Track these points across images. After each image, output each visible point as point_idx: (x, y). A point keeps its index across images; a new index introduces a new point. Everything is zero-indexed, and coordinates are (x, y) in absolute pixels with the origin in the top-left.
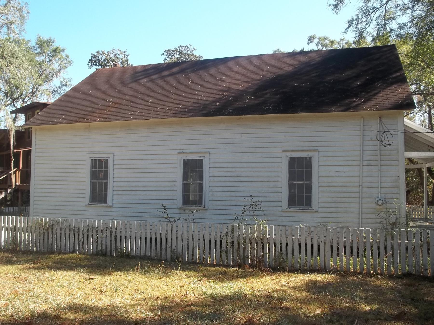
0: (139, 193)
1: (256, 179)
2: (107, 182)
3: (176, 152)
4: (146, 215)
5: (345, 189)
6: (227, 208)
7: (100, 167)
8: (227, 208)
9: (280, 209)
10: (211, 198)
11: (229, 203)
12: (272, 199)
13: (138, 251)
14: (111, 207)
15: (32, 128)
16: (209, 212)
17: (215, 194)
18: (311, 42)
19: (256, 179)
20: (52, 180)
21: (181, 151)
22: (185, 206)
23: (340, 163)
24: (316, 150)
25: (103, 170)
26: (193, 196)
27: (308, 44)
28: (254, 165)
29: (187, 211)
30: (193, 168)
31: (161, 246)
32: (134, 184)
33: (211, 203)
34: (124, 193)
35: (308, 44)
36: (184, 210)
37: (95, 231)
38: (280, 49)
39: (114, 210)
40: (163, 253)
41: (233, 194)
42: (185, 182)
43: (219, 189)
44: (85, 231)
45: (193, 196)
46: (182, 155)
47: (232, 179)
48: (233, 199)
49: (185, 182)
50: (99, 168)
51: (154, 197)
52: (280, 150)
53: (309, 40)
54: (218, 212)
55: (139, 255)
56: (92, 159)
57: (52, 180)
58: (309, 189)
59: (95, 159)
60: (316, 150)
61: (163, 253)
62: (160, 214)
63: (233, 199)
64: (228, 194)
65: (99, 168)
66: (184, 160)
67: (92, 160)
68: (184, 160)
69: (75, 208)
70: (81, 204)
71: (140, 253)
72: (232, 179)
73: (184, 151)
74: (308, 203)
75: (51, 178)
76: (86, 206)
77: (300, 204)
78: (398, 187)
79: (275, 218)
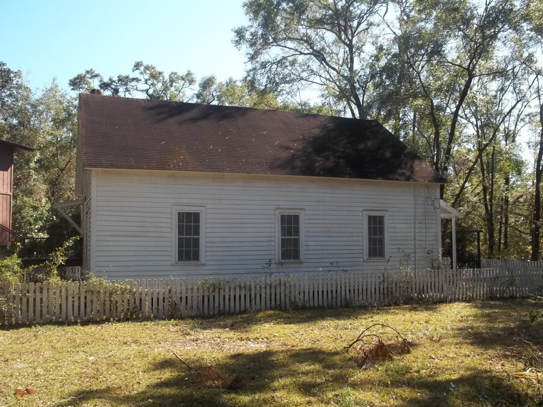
0: (234, 249)
1: (342, 234)
2: (198, 239)
3: (274, 207)
4: (241, 271)
5: (405, 242)
6: (321, 260)
7: (189, 221)
8: (321, 260)
9: (361, 260)
10: (306, 252)
11: (321, 256)
12: (355, 251)
13: (311, 303)
14: (204, 265)
15: (90, 171)
16: (304, 265)
17: (310, 248)
18: (137, 69)
19: (342, 234)
20: (124, 236)
21: (278, 207)
22: (284, 261)
23: (402, 222)
24: (387, 211)
25: (192, 224)
26: (291, 250)
27: (133, 71)
28: (341, 222)
29: (285, 266)
30: (290, 224)
31: (261, 302)
32: (229, 240)
33: (306, 256)
34: (218, 249)
35: (133, 71)
36: (282, 264)
37: (268, 287)
38: (94, 69)
39: (206, 268)
40: (334, 301)
41: (325, 248)
42: (296, 237)
43: (313, 243)
44: (258, 287)
45: (291, 250)
46: (279, 211)
47: (323, 234)
48: (325, 252)
49: (296, 237)
50: (189, 223)
51: (251, 253)
52: (361, 209)
53: (135, 66)
54: (312, 265)
55: (312, 306)
56: (180, 211)
57: (124, 236)
58: (197, 242)
59: (183, 211)
60: (387, 211)
61: (334, 301)
62: (265, 270)
63: (325, 252)
64: (321, 248)
65: (189, 223)
66: (282, 216)
67: (179, 213)
68: (282, 216)
69: (157, 268)
70: (165, 263)
71: (323, 303)
72: (323, 234)
73: (281, 207)
74: (196, 257)
75: (122, 234)
76: (172, 265)
77: (188, 258)
78: (436, 240)
79: (359, 267)
